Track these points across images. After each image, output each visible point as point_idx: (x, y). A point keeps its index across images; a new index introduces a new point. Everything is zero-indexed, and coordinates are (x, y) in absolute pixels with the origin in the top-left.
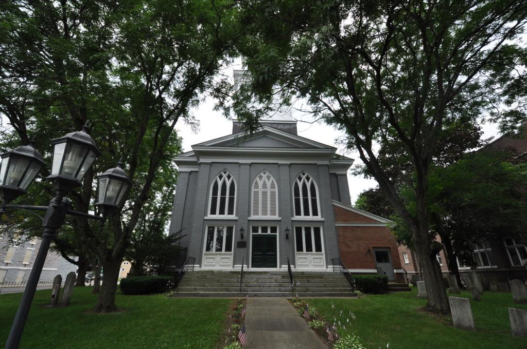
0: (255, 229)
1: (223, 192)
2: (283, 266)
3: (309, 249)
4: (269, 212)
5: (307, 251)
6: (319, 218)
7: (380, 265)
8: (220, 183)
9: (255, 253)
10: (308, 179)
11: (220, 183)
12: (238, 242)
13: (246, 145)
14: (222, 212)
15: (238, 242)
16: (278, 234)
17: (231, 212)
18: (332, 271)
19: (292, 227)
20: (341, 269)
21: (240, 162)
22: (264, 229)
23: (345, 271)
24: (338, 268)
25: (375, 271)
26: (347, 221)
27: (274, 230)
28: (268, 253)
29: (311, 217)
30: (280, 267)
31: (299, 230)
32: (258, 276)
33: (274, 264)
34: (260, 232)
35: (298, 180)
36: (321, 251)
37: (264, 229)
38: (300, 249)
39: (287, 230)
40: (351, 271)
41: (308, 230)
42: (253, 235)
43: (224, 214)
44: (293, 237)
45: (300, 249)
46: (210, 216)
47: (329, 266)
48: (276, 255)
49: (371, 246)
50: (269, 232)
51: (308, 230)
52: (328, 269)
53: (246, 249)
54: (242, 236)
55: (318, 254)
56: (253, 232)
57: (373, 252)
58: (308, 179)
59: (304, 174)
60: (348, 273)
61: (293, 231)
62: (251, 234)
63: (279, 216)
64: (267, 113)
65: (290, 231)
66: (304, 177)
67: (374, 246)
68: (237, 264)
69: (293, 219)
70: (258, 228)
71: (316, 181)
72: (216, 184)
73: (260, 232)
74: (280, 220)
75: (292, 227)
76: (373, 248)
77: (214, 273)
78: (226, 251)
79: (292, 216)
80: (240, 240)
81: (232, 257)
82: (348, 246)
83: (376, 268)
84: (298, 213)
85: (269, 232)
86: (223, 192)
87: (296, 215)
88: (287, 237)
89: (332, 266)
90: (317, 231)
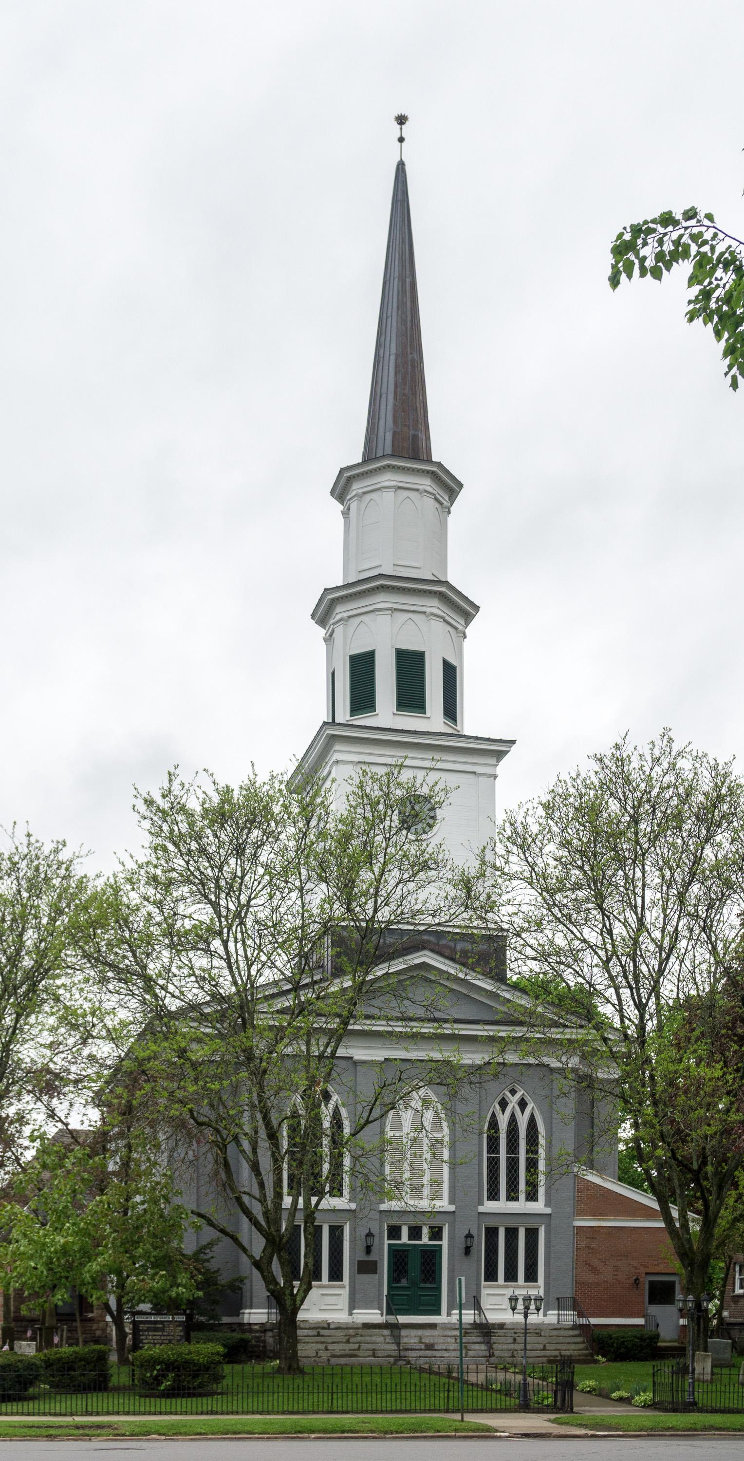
0: (395, 1232)
1: (513, 1147)
2: (355, 1311)
3: (511, 1276)
4: (522, 1196)
5: (507, 1279)
6: (539, 1206)
7: (654, 1310)
8: (503, 1121)
9: (394, 1285)
10: (523, 1104)
11: (503, 1121)
12: (360, 1263)
13: (373, 1002)
14: (512, 1196)
15: (360, 1263)
16: (445, 1243)
17: (532, 1196)
18: (556, 1322)
19: (479, 1228)
20: (576, 1317)
21: (356, 1058)
22: (415, 1232)
23: (583, 1321)
24: (569, 1317)
25: (641, 1321)
26: (601, 1214)
27: (436, 1234)
28: (423, 1285)
29: (521, 1206)
30: (449, 1314)
31: (492, 1233)
32: (420, 1332)
33: (435, 1308)
34: (405, 1239)
35: (498, 1107)
36: (536, 1280)
37: (415, 1232)
38: (491, 1276)
39: (370, 1235)
40: (594, 1321)
41: (511, 1234)
42: (389, 1245)
43: (516, 1199)
44: (480, 1251)
45: (491, 1276)
46: (490, 1206)
47: (550, 1312)
48: (439, 1289)
49: (643, 1270)
50: (425, 1240)
51: (511, 1234)
52: (548, 1317)
53: (376, 1276)
54: (368, 1250)
55: (529, 1287)
56: (388, 1239)
57: (645, 1282)
58: (523, 1104)
59: (513, 1092)
60: (588, 1326)
61: (480, 1236)
62: (387, 1242)
63: (452, 1202)
64: (15, 851)
65: (376, 1239)
66: (513, 1101)
67: (648, 1271)
68: (359, 1308)
69: (481, 1209)
70: (420, 1228)
71: (542, 1113)
72: (494, 1124)
73: (405, 1239)
74: (454, 1212)
75: (479, 1228)
76: (647, 1274)
77: (332, 1326)
78: (526, 1281)
79: (481, 1203)
80: (364, 1258)
81: (345, 1293)
82: (594, 1270)
83: (643, 1317)
84: (493, 1195)
85: (425, 1240)
86: (513, 1147)
87: (489, 1199)
88: (467, 1251)
89: (556, 1312)
90: (532, 1234)
